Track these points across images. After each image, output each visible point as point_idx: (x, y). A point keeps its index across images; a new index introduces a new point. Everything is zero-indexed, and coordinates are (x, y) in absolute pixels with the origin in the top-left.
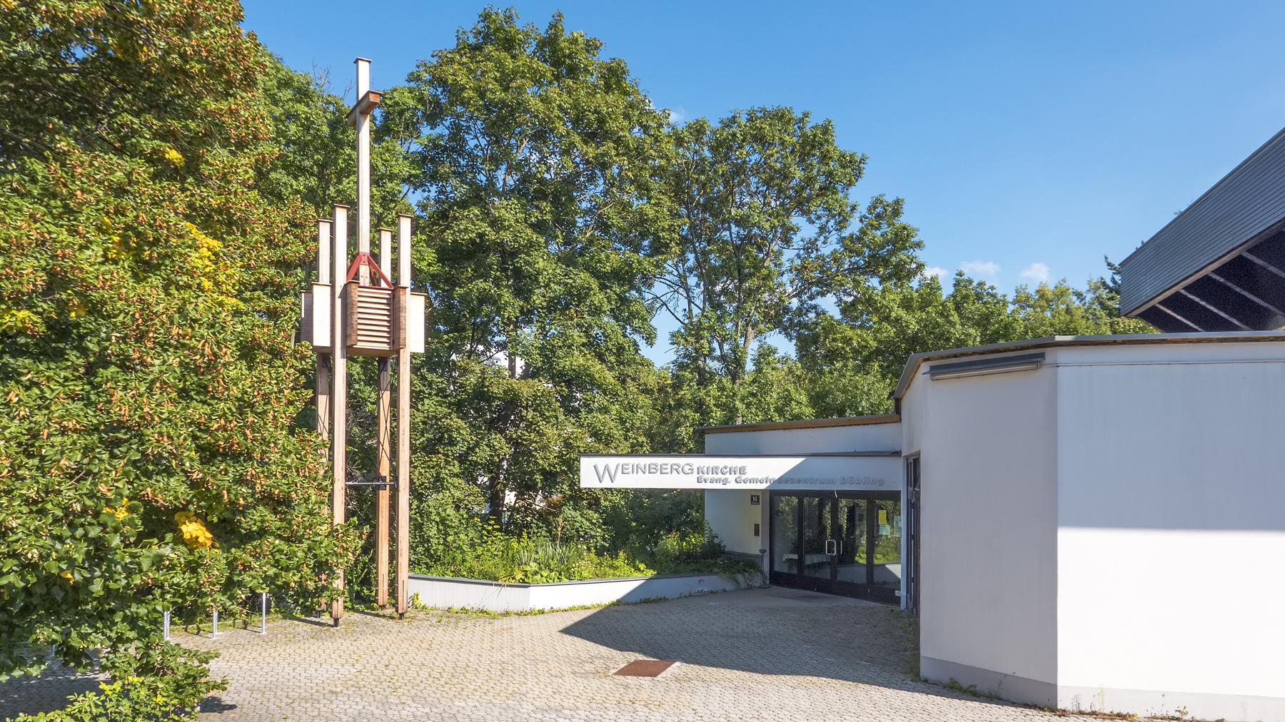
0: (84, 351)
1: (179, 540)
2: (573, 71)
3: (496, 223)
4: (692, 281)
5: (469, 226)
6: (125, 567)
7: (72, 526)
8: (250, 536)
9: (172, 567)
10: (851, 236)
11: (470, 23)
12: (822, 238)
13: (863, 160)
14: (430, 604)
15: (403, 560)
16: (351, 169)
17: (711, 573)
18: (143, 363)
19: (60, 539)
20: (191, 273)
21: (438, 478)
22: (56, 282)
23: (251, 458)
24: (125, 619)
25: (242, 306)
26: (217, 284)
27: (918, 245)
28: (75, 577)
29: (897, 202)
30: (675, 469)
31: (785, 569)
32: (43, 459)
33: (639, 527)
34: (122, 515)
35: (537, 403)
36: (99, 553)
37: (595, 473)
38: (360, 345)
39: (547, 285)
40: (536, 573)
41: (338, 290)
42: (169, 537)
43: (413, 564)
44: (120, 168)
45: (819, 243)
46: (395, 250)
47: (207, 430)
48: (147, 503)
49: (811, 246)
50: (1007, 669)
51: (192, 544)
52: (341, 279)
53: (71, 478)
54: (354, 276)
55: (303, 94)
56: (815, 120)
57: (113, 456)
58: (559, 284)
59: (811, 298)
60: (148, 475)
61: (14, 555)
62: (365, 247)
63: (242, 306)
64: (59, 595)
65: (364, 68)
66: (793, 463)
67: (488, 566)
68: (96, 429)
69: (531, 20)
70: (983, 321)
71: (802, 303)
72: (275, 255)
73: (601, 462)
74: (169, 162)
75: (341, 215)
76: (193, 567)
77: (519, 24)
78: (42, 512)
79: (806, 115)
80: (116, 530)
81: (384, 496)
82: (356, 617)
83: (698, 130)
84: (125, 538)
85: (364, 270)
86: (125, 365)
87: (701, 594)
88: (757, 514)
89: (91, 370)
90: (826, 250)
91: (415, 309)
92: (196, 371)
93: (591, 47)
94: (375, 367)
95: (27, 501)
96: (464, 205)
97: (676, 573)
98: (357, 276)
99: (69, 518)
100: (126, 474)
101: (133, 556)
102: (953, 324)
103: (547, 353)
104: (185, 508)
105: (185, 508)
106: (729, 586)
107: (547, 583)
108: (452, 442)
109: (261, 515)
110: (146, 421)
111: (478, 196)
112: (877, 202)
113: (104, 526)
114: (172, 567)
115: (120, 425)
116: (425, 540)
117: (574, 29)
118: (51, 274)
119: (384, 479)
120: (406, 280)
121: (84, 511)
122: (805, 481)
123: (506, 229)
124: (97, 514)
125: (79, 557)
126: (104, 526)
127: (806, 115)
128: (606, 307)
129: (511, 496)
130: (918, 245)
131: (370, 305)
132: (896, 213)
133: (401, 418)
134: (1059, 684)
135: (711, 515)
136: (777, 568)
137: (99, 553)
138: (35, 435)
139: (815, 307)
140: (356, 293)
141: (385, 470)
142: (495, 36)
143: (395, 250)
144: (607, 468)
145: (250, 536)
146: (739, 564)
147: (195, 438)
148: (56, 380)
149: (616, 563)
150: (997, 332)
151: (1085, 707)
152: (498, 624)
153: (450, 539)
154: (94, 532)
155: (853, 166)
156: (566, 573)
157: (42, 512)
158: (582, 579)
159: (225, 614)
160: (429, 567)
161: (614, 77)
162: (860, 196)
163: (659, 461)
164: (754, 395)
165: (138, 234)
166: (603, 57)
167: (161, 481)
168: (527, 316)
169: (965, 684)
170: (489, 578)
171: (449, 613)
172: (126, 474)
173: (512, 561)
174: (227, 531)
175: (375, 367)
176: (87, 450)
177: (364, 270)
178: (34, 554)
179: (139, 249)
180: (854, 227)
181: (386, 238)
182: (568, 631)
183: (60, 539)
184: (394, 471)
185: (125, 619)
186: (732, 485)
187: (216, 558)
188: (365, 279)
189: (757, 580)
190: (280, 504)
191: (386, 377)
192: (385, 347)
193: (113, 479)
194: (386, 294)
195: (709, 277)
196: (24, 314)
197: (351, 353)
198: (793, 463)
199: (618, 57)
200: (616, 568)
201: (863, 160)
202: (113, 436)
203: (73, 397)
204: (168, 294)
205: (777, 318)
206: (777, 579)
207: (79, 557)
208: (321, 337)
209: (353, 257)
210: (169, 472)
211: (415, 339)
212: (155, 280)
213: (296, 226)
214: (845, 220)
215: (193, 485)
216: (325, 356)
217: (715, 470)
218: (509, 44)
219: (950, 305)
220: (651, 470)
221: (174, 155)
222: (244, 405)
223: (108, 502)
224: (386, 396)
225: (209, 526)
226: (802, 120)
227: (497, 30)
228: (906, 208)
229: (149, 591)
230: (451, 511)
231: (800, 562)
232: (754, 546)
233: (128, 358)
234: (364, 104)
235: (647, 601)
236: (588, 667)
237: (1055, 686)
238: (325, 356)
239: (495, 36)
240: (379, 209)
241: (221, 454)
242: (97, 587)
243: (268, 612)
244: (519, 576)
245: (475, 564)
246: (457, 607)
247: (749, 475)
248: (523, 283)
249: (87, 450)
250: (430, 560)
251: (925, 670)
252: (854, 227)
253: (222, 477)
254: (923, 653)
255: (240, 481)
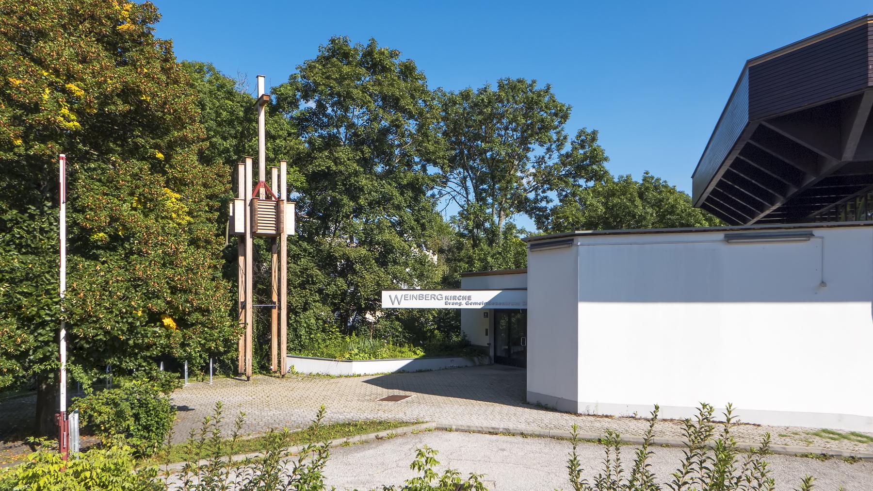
0: (125, 249)
1: (162, 325)
2: (385, 69)
3: (336, 161)
4: (469, 183)
5: (323, 162)
6: (142, 335)
7: (122, 318)
8: (193, 325)
9: (160, 336)
10: (567, 153)
11: (326, 44)
12: (548, 156)
13: (569, 108)
14: (300, 372)
15: (284, 346)
16: (256, 133)
17: (458, 356)
18: (147, 253)
19: (118, 322)
20: (167, 211)
21: (306, 303)
22: (113, 219)
23: (191, 292)
24: (141, 357)
25: (192, 220)
26: (178, 215)
27: (606, 159)
28: (123, 338)
29: (594, 133)
30: (433, 297)
31: (503, 355)
32: (110, 292)
33: (411, 328)
34: (140, 314)
35: (363, 261)
36: (132, 328)
37: (389, 300)
38: (259, 231)
39: (370, 193)
40: (357, 354)
41: (248, 202)
42: (158, 324)
43: (289, 349)
44: (136, 165)
45: (546, 159)
46: (279, 176)
47: (173, 281)
48: (149, 310)
49: (541, 160)
50: (559, 395)
51: (167, 328)
52: (249, 196)
53: (121, 299)
54: (256, 194)
55: (230, 94)
56: (539, 87)
57: (136, 291)
58: (376, 192)
59: (544, 192)
60: (150, 299)
61: (101, 328)
62: (262, 177)
63: (192, 220)
64: (117, 345)
65: (261, 80)
66: (495, 293)
67: (332, 351)
68: (129, 280)
69: (357, 41)
70: (658, 204)
71: (537, 195)
72: (209, 192)
73: (393, 293)
74: (157, 159)
75: (249, 162)
76: (168, 336)
77: (351, 46)
78: (112, 312)
79: (534, 82)
80: (138, 319)
81: (275, 312)
82: (260, 376)
83: (465, 96)
84: (141, 323)
85: (262, 191)
86: (140, 253)
87: (452, 368)
88: (487, 323)
89: (127, 256)
90: (550, 163)
91: (289, 211)
92: (169, 255)
93: (393, 54)
94: (272, 241)
95: (106, 308)
96: (320, 150)
97: (438, 356)
98: (258, 195)
99: (122, 315)
100: (141, 298)
101: (145, 330)
102: (636, 207)
103: (368, 232)
104: (164, 313)
105: (164, 313)
106: (469, 364)
107: (362, 360)
108: (314, 283)
109: (197, 316)
110: (149, 277)
111: (331, 143)
112: (582, 132)
113: (134, 318)
114: (160, 336)
115: (139, 279)
116: (298, 336)
117: (383, 46)
118: (111, 217)
119: (275, 303)
120: (284, 196)
121: (126, 313)
122: (500, 304)
123: (341, 163)
124: (131, 313)
125: (125, 329)
126: (134, 318)
127: (534, 82)
128: (403, 204)
129: (343, 315)
130: (606, 159)
131: (265, 210)
132: (594, 139)
133: (281, 269)
134: (579, 401)
135: (465, 324)
136: (499, 354)
137: (132, 328)
138: (107, 282)
139: (546, 197)
140: (257, 203)
141: (275, 298)
142: (338, 52)
143: (279, 176)
144: (396, 297)
145: (193, 325)
146: (481, 351)
147: (168, 283)
148: (114, 260)
149: (403, 349)
150: (666, 210)
151: (591, 413)
152: (332, 380)
153: (312, 336)
154: (130, 320)
155: (563, 115)
156: (374, 355)
157: (112, 312)
158: (383, 359)
159: (191, 373)
160: (300, 351)
161: (407, 71)
162: (571, 129)
163: (424, 293)
164: (500, 253)
165: (145, 197)
166: (402, 59)
167: (155, 301)
168: (358, 211)
169: (543, 404)
170: (331, 357)
171: (311, 376)
172: (141, 298)
173: (345, 348)
174: (182, 323)
175: (272, 241)
176: (127, 289)
177: (262, 191)
178: (109, 328)
179: (145, 203)
180: (567, 148)
181: (275, 172)
182: (367, 382)
183: (117, 322)
184: (279, 300)
185: (141, 357)
186: (464, 306)
187: (178, 335)
188: (263, 196)
189: (486, 361)
190: (205, 311)
191: (274, 247)
192: (274, 232)
193: (136, 301)
194: (274, 204)
195: (479, 180)
196: (101, 234)
197: (254, 235)
198: (495, 293)
199: (412, 58)
200: (403, 352)
201: (569, 108)
202: (135, 283)
203: (120, 267)
204: (157, 221)
205: (522, 205)
206: (498, 360)
207: (125, 329)
208: (239, 228)
209: (255, 184)
210: (159, 299)
211: (289, 227)
212: (152, 216)
213: (220, 176)
214: (562, 144)
215: (168, 303)
216: (242, 237)
217: (454, 298)
218: (345, 56)
219: (635, 194)
220: (421, 298)
221: (160, 156)
222: (189, 269)
223: (135, 309)
224: (275, 256)
225: (175, 320)
226: (531, 85)
227: (339, 49)
228: (599, 136)
229: (151, 346)
230: (313, 321)
231: (509, 350)
232: (484, 340)
233: (141, 251)
234: (261, 101)
235: (420, 371)
236: (367, 398)
237: (576, 402)
238: (242, 237)
239: (338, 52)
240: (272, 156)
241: (180, 291)
242: (131, 342)
243: (214, 374)
244: (347, 356)
245: (325, 350)
246: (314, 373)
247: (473, 301)
248: (354, 192)
249: (127, 289)
250: (298, 347)
251: (529, 399)
252: (567, 148)
253: (180, 298)
254: (528, 389)
255: (187, 301)
